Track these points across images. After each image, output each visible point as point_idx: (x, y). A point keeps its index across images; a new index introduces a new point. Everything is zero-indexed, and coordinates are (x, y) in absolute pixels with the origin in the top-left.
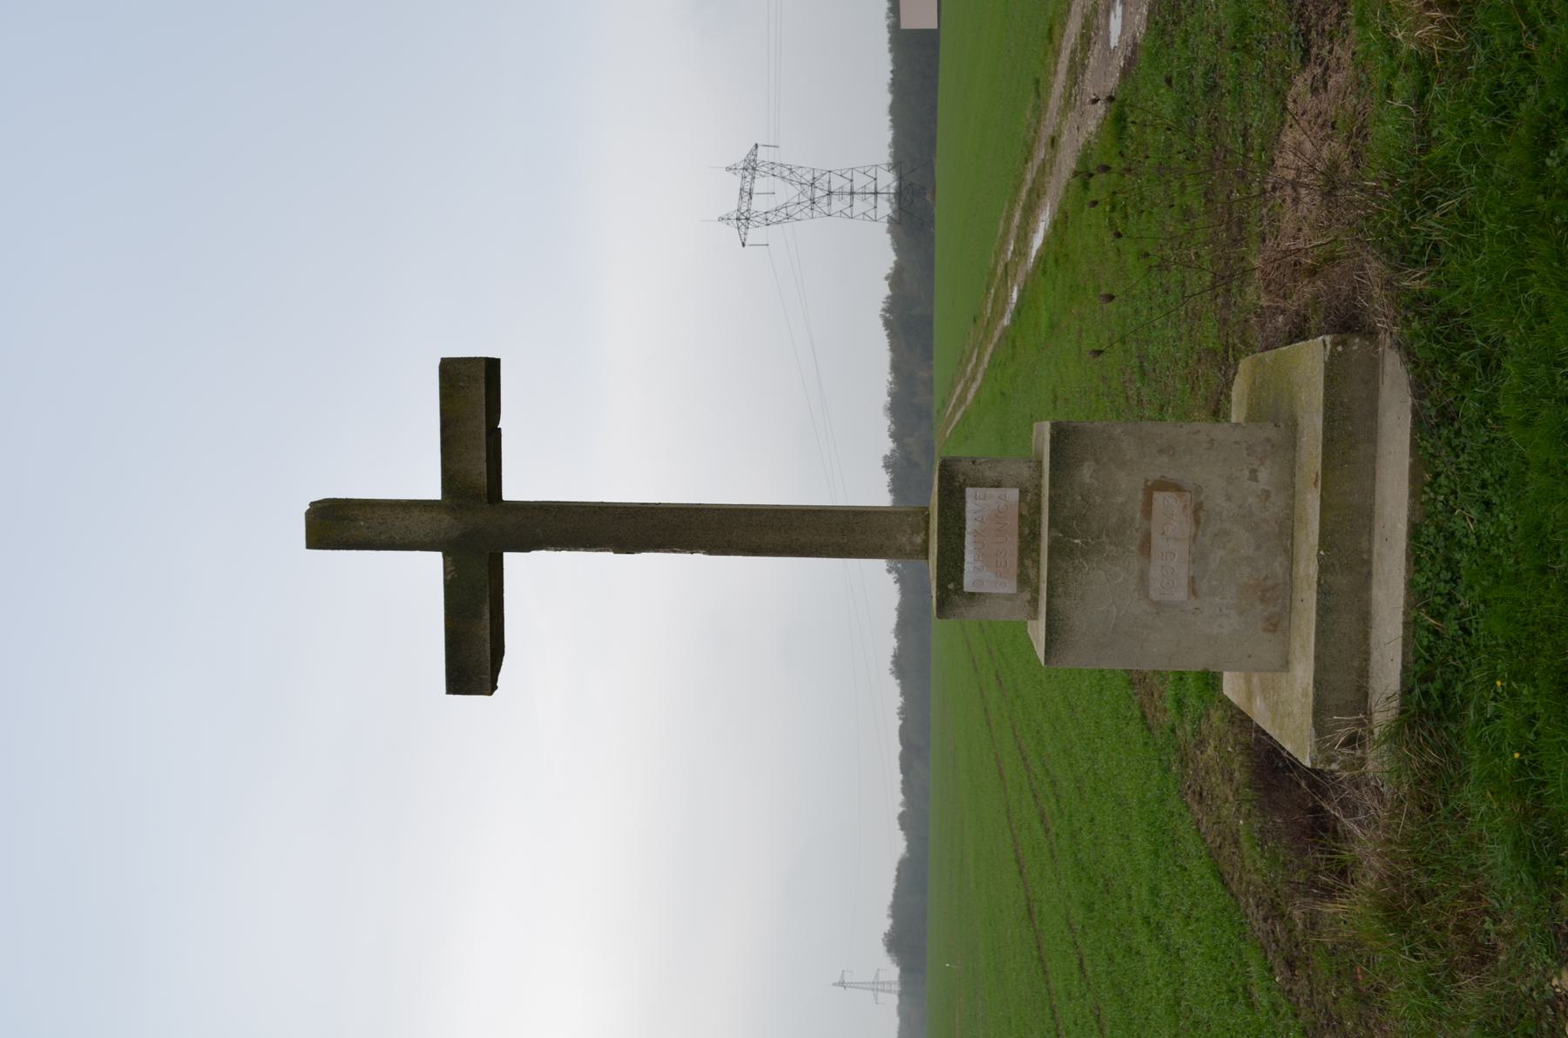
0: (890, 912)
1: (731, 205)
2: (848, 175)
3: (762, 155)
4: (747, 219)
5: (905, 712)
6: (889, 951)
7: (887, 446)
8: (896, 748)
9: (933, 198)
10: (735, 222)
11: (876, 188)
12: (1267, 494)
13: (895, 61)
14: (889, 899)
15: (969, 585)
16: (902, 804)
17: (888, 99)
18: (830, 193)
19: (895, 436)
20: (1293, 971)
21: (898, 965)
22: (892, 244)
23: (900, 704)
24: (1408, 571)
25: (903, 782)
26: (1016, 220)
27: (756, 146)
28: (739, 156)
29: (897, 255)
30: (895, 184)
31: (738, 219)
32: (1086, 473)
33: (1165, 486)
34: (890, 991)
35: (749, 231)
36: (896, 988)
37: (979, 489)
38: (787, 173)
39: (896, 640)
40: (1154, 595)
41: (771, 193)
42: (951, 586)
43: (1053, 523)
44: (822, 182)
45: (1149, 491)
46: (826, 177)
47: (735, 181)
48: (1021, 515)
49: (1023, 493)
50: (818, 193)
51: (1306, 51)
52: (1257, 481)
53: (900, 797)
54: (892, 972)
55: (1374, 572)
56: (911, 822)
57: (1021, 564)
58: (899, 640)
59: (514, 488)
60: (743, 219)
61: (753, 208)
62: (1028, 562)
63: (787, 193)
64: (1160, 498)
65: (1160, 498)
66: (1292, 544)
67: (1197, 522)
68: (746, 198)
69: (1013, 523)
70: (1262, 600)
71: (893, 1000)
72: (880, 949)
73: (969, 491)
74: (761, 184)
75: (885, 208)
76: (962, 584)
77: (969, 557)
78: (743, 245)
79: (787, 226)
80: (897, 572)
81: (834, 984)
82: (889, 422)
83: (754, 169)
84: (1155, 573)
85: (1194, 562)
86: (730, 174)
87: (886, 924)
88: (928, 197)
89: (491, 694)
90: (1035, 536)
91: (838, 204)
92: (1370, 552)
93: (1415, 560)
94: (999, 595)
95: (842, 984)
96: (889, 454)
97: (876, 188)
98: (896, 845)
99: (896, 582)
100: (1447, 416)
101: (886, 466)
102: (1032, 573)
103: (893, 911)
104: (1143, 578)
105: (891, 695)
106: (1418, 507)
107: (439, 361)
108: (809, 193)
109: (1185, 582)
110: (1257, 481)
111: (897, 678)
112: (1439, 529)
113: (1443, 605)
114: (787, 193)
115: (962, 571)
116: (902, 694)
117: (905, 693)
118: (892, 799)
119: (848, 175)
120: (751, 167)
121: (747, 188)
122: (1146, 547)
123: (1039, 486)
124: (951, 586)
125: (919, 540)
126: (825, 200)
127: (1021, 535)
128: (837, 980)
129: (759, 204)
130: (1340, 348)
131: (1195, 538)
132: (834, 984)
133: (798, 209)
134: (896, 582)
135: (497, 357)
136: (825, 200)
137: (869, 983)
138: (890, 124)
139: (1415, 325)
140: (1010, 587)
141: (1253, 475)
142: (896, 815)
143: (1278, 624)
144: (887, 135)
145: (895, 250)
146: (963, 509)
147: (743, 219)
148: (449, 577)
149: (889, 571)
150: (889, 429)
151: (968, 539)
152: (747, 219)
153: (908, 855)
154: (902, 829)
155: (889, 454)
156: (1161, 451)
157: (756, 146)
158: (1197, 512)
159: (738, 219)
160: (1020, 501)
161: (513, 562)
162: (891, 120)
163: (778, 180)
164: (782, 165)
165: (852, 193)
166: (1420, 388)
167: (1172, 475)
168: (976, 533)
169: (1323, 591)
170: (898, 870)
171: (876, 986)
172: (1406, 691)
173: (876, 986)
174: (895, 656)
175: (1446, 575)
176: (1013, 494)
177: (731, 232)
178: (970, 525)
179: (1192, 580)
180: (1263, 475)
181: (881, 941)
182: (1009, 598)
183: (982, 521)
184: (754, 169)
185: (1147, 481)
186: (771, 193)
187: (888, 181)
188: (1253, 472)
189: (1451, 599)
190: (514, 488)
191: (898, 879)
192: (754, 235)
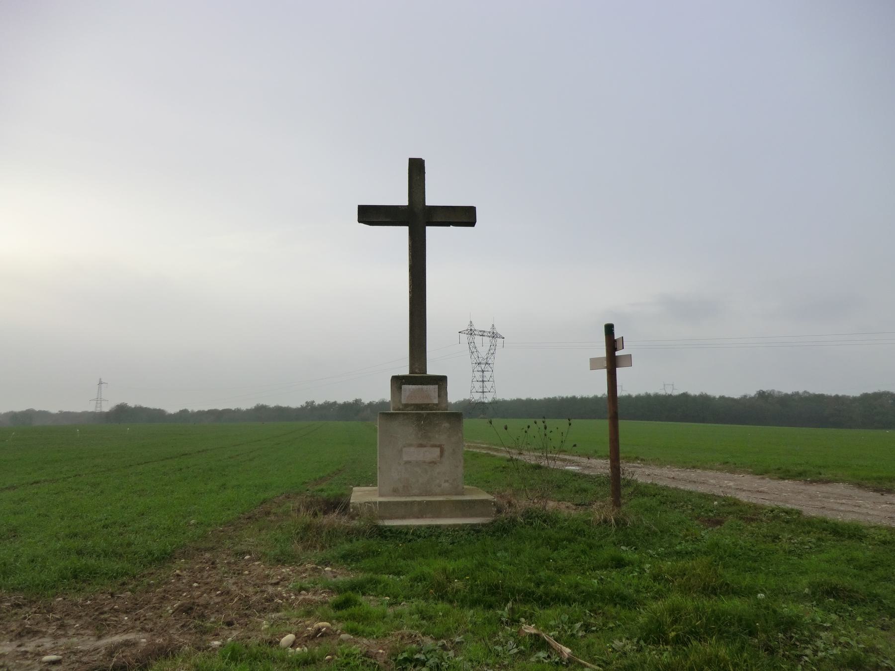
0: (138, 406)
1: (477, 327)
2: (491, 380)
3: (499, 340)
4: (471, 334)
5: (238, 411)
6: (118, 406)
7: (366, 401)
8: (220, 408)
9: (482, 418)
10: (470, 328)
11: (485, 392)
12: (440, 486)
13: (541, 400)
14: (144, 405)
15: (404, 387)
16: (192, 411)
17: (524, 398)
18: (483, 371)
19: (370, 405)
20: (247, 519)
21: (110, 410)
22: (459, 401)
23: (242, 409)
24: (425, 525)
25: (204, 411)
26: (482, 445)
27: (504, 338)
28: (499, 330)
29: (454, 403)
30: (486, 401)
31: (471, 330)
32: (446, 425)
33: (442, 452)
34: (96, 407)
35: (466, 335)
36: (98, 410)
37: (437, 390)
38: (492, 352)
39: (273, 406)
40: (405, 449)
41: (483, 345)
42: (404, 381)
43: (428, 414)
44: (488, 368)
45: (440, 446)
46: (490, 370)
47: (488, 328)
48: (429, 404)
49: (437, 405)
50: (483, 366)
51: (579, 505)
52: (444, 482)
53: (196, 410)
54: (106, 408)
55: (419, 519)
56: (184, 416)
57: (412, 405)
58: (273, 408)
59: (430, 231)
60: (471, 332)
61: (476, 337)
62: (412, 407)
63: (483, 351)
64: (438, 450)
65: (438, 450)
66: (423, 495)
67: (430, 463)
68: (480, 334)
69: (426, 401)
70: (404, 486)
71: (91, 408)
72: (118, 402)
73: (437, 386)
74: (487, 340)
75: (477, 397)
76: (404, 384)
77: (414, 387)
78: (460, 332)
79: (468, 352)
80: (306, 406)
81: (100, 379)
82: (377, 401)
83: (493, 337)
84: (412, 449)
85: (417, 462)
86: (491, 326)
87: (132, 404)
88: (482, 416)
89: (358, 221)
90: (422, 410)
91: (478, 375)
92: (426, 518)
93: (429, 527)
94: (401, 397)
95: (101, 383)
96: (362, 401)
97: (485, 392)
98: (172, 408)
99: (301, 406)
100: (478, 531)
101: (356, 401)
102: (409, 408)
103: (138, 407)
104: (410, 445)
105: (246, 404)
106: (446, 527)
107: (475, 206)
108: (483, 362)
109: (409, 459)
110: (444, 482)
111: (255, 407)
112: (440, 533)
113: (417, 534)
114: (483, 351)
115: (409, 384)
116: (247, 410)
117: (248, 411)
118: (196, 406)
119: (491, 380)
120: (494, 335)
121: (485, 334)
122: (421, 446)
123: (439, 410)
124: (404, 381)
125: (417, 371)
126: (480, 369)
127: (422, 404)
128: (103, 381)
129: (478, 339)
130: (493, 504)
131: (424, 462)
132: (100, 379)
133: (476, 357)
134: (301, 406)
135: (357, 207)
136: (480, 369)
137: (101, 396)
138: (513, 399)
139: (505, 521)
140: (404, 401)
141: (446, 481)
142: (187, 408)
143: (395, 492)
144: (508, 398)
145: (456, 403)
146: (430, 384)
147: (471, 332)
148: (400, 208)
149: (307, 402)
150: (374, 401)
151: (420, 386)
152: (471, 334)
153: (167, 414)
154: (180, 411)
155: (362, 401)
156: (454, 450)
157: (504, 338)
158: (433, 463)
159: (471, 330)
160: (434, 404)
161: (406, 229)
162: (514, 399)
163: (489, 347)
164: (495, 349)
165: (483, 381)
166: (484, 525)
167: (446, 454)
168: (422, 389)
169: (412, 503)
170: (160, 410)
171: (99, 400)
172: (386, 527)
173: (99, 400)
174: (266, 406)
175: (426, 535)
176: (436, 401)
177: (466, 327)
178: (425, 387)
179: (410, 462)
180: (447, 484)
181: (123, 402)
182: (400, 401)
183: (426, 391)
184: (493, 337)
185: (444, 445)
186: (483, 345)
187: (488, 398)
188: (448, 481)
189: (419, 537)
190: (430, 231)
191: (155, 410)
192: (464, 337)
